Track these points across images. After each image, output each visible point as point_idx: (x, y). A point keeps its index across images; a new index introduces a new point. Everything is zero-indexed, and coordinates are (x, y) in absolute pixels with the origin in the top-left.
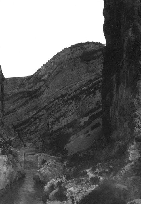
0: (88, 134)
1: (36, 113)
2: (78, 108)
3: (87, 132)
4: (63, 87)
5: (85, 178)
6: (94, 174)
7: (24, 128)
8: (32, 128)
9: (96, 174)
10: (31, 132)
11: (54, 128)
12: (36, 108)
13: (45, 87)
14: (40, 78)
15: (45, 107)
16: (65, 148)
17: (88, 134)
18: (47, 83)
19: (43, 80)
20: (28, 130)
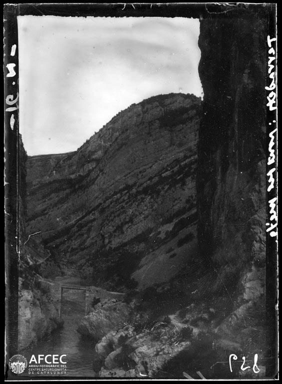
0: (172, 253)
1: (83, 217)
3: (170, 250)
4: (129, 171)
6: (183, 323)
8: (76, 242)
10: (73, 250)
11: (113, 243)
12: (82, 207)
14: (89, 156)
15: (98, 206)
16: (132, 277)
17: (172, 253)
18: (101, 165)
19: (93, 160)
20: (68, 247)
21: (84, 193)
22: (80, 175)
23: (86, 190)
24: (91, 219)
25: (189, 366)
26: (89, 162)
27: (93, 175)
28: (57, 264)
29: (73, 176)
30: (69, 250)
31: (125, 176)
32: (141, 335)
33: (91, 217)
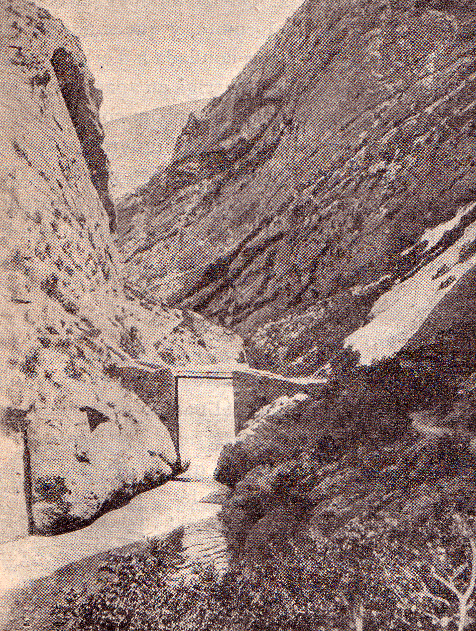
0: (444, 278)
1: (254, 234)
2: (410, 189)
3: (442, 271)
4: (353, 116)
5: (397, 446)
6: (445, 425)
7: (211, 297)
8: (244, 292)
9: (452, 424)
10: (238, 309)
11: (321, 281)
12: (247, 215)
13: (282, 125)
14: (259, 94)
15: (285, 206)
16: (347, 342)
17: (444, 278)
18: (287, 110)
19: (272, 100)
20: (228, 302)
21: (253, 177)
22: (242, 140)
23: (257, 171)
24: (271, 234)
25: (87, 627)
26: (261, 105)
27: (269, 138)
28: (198, 339)
29: (226, 144)
30: (231, 310)
31: (342, 129)
32: (329, 467)
33: (272, 230)
